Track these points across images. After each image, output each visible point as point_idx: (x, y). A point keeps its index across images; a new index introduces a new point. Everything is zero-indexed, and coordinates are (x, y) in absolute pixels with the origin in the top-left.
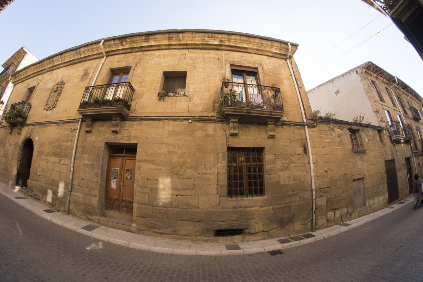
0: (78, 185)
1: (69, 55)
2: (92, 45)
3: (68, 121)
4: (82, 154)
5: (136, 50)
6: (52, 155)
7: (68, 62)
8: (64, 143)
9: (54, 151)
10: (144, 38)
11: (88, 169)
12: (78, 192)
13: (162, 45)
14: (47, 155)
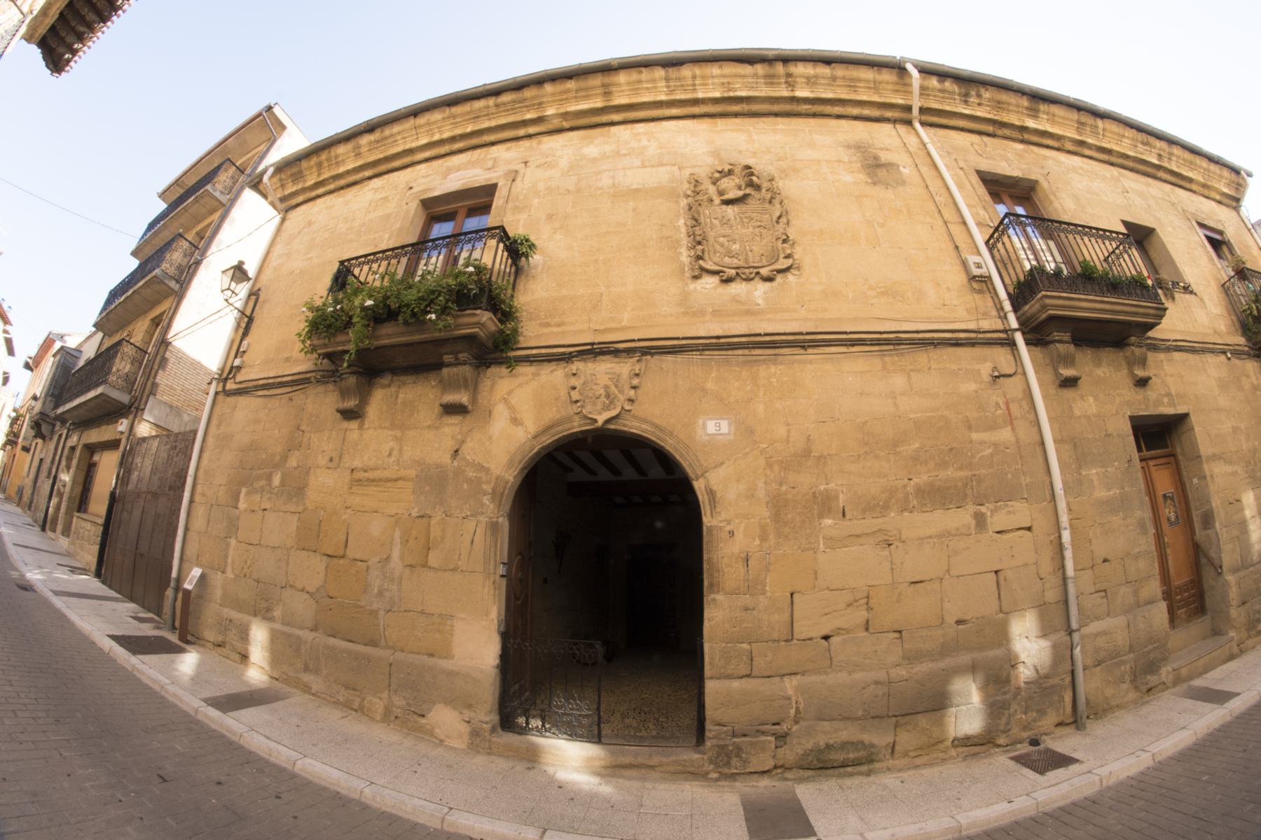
0: (1092, 589)
2: (851, 66)
4: (1080, 467)
5: (1007, 132)
7: (716, 101)
10: (1025, 102)
11: (1115, 518)
12: (1098, 618)
13: (1069, 138)
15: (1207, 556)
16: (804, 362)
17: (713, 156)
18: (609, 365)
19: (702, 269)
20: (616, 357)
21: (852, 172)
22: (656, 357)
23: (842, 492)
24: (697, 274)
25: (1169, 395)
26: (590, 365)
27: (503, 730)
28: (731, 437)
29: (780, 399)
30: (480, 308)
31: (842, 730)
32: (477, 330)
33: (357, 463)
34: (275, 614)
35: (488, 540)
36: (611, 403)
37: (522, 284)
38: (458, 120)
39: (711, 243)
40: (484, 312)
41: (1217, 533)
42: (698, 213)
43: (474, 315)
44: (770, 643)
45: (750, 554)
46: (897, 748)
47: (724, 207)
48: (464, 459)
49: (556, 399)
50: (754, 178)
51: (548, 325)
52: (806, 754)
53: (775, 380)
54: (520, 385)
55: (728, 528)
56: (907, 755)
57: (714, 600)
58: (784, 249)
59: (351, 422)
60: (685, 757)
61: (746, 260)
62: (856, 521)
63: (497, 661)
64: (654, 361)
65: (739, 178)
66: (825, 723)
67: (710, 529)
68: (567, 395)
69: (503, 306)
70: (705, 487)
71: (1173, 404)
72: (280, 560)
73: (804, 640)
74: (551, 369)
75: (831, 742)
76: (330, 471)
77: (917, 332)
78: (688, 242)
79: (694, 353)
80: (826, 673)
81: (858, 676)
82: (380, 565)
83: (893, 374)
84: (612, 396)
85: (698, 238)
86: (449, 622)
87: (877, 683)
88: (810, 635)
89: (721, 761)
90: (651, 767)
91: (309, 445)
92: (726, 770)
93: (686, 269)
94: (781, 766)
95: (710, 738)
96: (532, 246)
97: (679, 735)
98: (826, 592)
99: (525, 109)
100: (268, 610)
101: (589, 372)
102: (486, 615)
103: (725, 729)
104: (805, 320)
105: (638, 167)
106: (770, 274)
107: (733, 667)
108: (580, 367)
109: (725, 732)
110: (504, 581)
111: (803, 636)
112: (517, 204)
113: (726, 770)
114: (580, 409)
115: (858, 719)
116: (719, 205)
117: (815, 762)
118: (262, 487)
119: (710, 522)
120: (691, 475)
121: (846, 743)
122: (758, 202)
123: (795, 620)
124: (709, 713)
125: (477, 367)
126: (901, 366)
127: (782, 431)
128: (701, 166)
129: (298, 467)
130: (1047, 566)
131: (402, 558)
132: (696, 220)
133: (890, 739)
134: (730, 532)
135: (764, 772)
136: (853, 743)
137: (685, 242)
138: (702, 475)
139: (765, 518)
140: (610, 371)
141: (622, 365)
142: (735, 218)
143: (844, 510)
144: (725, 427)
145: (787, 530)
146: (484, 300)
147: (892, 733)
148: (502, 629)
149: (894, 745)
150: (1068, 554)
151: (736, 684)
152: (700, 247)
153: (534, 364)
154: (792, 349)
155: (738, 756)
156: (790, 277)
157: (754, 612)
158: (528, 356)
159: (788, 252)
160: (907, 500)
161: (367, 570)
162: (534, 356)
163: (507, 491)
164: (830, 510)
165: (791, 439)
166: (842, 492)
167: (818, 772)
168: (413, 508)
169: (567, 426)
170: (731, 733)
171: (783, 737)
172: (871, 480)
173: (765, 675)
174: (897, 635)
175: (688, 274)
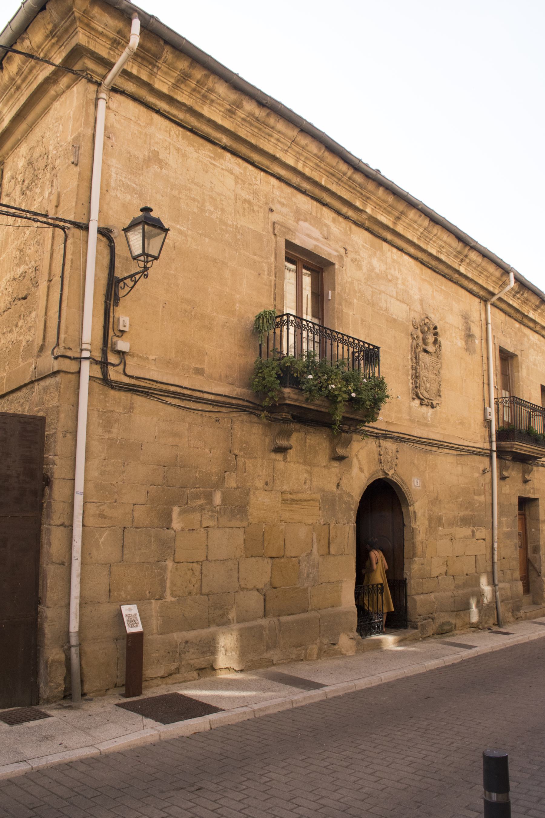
1: (445, 242)
3: (475, 449)
6: (459, 523)
8: (476, 497)
9: (461, 514)
14: (451, 524)
15: (533, 566)
25: (533, 488)
33: (285, 488)
34: (230, 617)
38: (322, 165)
41: (540, 557)
48: (342, 489)
59: (277, 454)
71: (534, 493)
72: (231, 570)
76: (266, 493)
77: (468, 446)
82: (306, 558)
86: (340, 585)
91: (245, 469)
99: (358, 195)
100: (222, 615)
118: (201, 506)
129: (238, 487)
130: (488, 557)
131: (318, 552)
150: (496, 553)
161: (299, 563)
168: (321, 519)
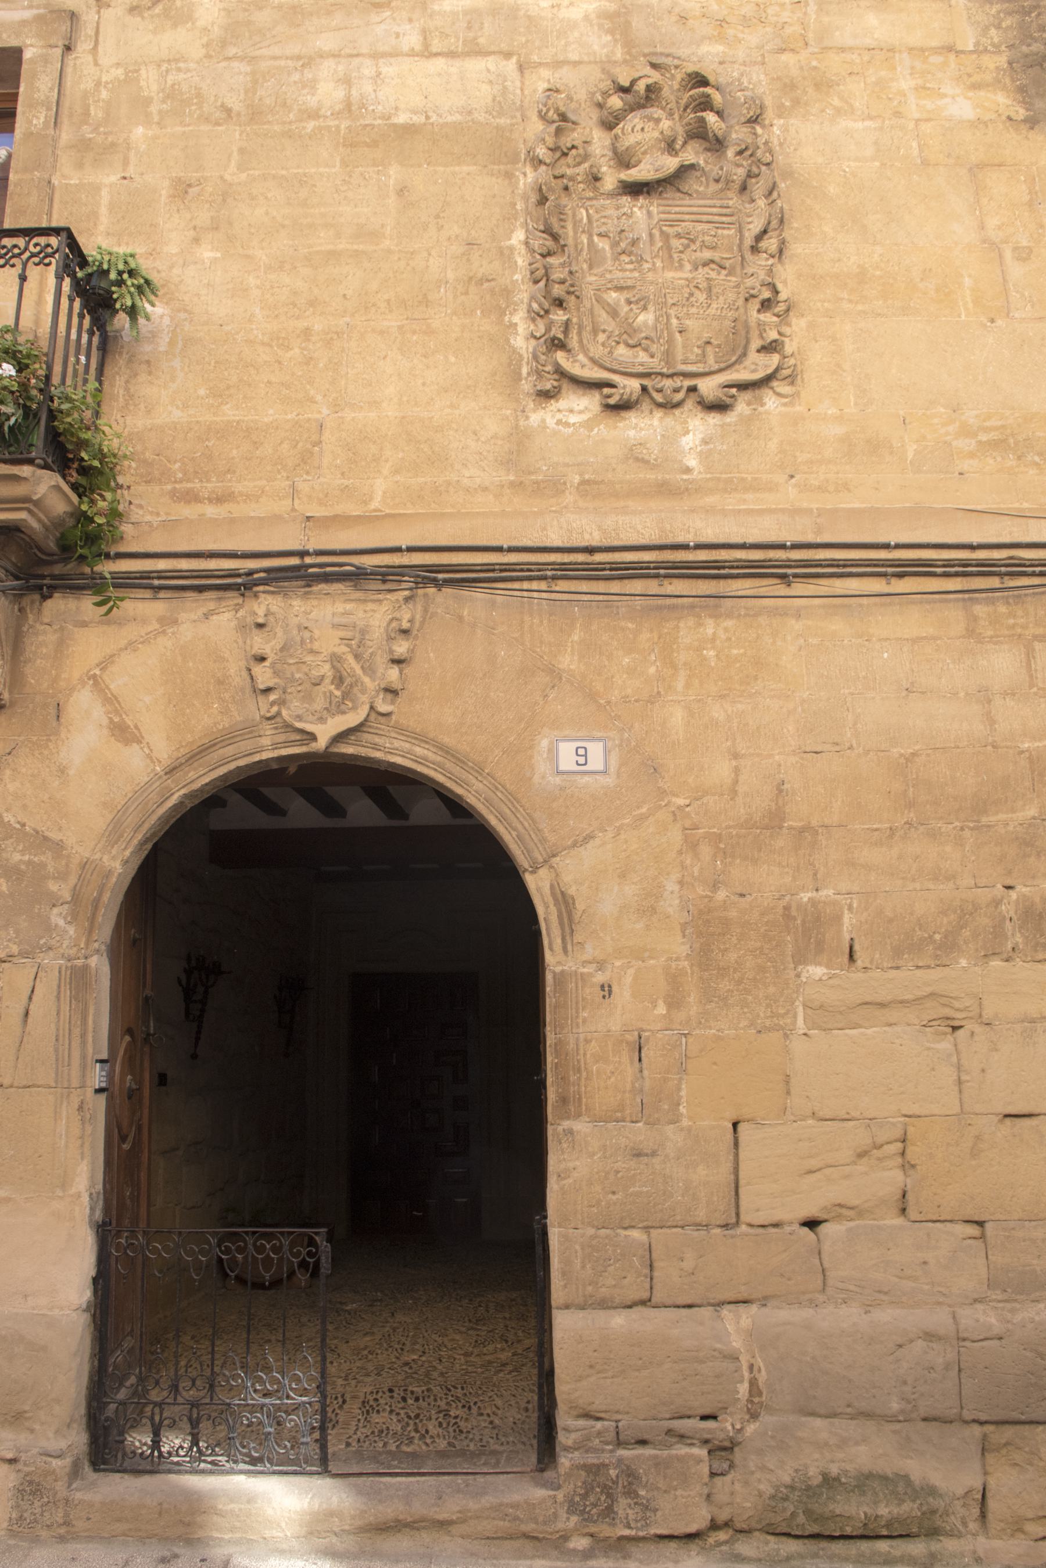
16: (783, 613)
17: (611, 32)
18: (340, 607)
19: (561, 373)
20: (356, 587)
21: (975, 87)
22: (447, 591)
23: (850, 908)
24: (548, 386)
26: (297, 604)
27: (96, 1470)
28: (610, 781)
29: (722, 697)
30: (30, 462)
31: (857, 1443)
32: (23, 515)
35: (65, 1008)
36: (346, 695)
37: (120, 382)
39: (587, 304)
40: (41, 472)
42: (560, 212)
43: (16, 478)
44: (688, 1230)
45: (645, 1034)
46: (992, 1504)
47: (626, 200)
49: (220, 682)
50: (711, 118)
51: (191, 497)
52: (779, 1497)
53: (712, 653)
54: (131, 646)
55: (600, 978)
56: (1021, 1530)
57: (570, 1132)
58: (761, 327)
60: (516, 1497)
61: (668, 356)
62: (877, 974)
63: (88, 1294)
64: (443, 599)
65: (671, 114)
66: (818, 1422)
67: (561, 979)
68: (245, 674)
69: (83, 455)
70: (552, 887)
73: (763, 1226)
74: (205, 610)
75: (834, 1470)
78: (533, 298)
79: (535, 585)
80: (813, 1304)
81: (885, 1315)
83: (990, 646)
84: (348, 681)
85: (557, 290)
87: (929, 1336)
88: (778, 1216)
89: (594, 1505)
90: (443, 1525)
92: (605, 1530)
93: (525, 370)
94: (727, 1524)
95: (567, 1449)
96: (146, 287)
97: (497, 1447)
98: (810, 1122)
101: (295, 621)
102: (64, 1186)
103: (599, 1425)
104: (796, 512)
105: (412, 53)
106: (720, 394)
107: (610, 1282)
108: (274, 608)
109: (599, 1434)
110: (102, 1098)
111: (762, 1218)
112: (87, 131)
113: (605, 1530)
114: (275, 709)
115: (892, 1419)
116: (611, 195)
117: (801, 1519)
119: (559, 963)
120: (521, 859)
121: (870, 1476)
122: (714, 187)
123: (742, 1182)
124: (563, 1388)
125: (18, 596)
126: (1013, 626)
127: (722, 770)
128: (576, 64)
132: (555, 237)
133: (972, 1480)
134: (602, 987)
135: (691, 1537)
136: (884, 1478)
137: (525, 296)
138: (545, 861)
139: (678, 959)
140: (343, 620)
141: (370, 606)
142: (651, 236)
143: (851, 948)
144: (567, 756)
145: (725, 985)
146: (38, 438)
147: (977, 1465)
148: (98, 1215)
149: (984, 1489)
151: (619, 1320)
152: (559, 316)
153: (162, 594)
154: (757, 582)
155: (630, 1493)
156: (771, 402)
157: (656, 1161)
158: (146, 575)
159: (773, 335)
160: (998, 932)
162: (161, 575)
163: (106, 897)
164: (820, 947)
165: (741, 789)
166: (850, 908)
167: (812, 1546)
169: (246, 746)
170: (611, 1436)
171: (724, 1449)
172: (918, 886)
173: (680, 1301)
174: (973, 1230)
175: (526, 386)
